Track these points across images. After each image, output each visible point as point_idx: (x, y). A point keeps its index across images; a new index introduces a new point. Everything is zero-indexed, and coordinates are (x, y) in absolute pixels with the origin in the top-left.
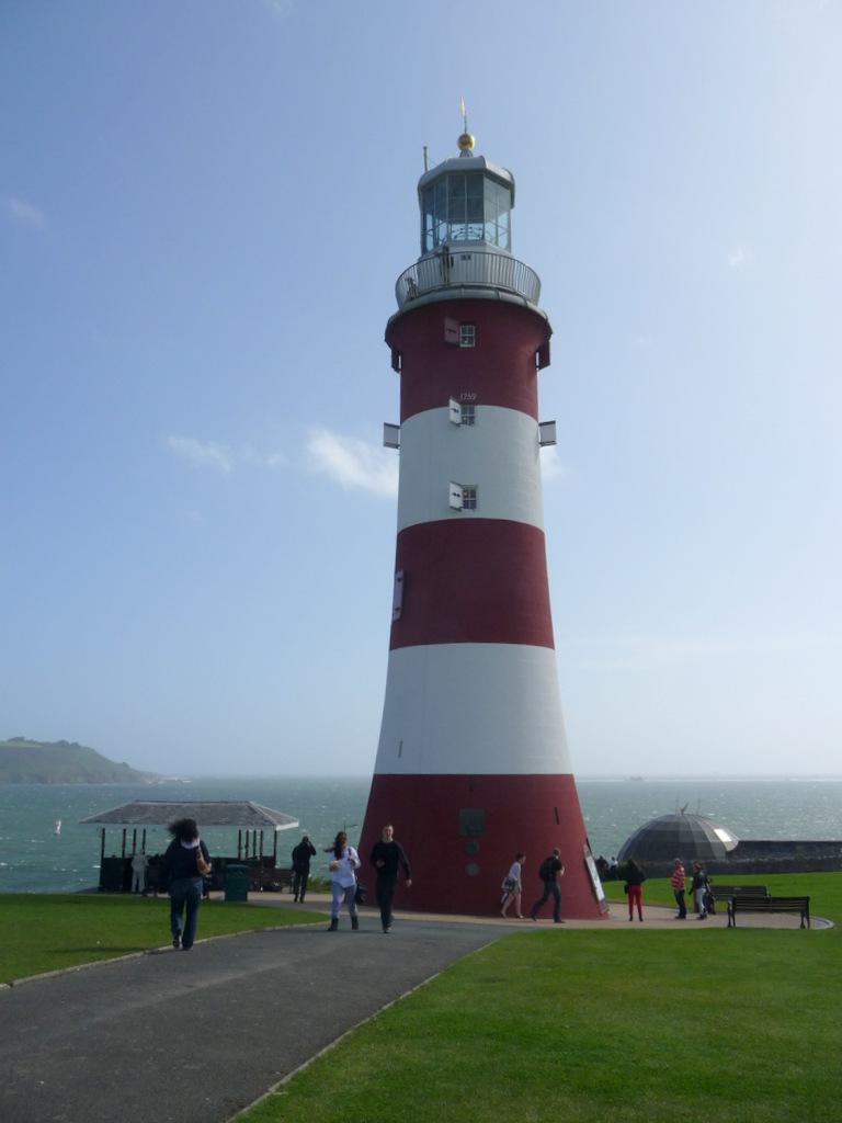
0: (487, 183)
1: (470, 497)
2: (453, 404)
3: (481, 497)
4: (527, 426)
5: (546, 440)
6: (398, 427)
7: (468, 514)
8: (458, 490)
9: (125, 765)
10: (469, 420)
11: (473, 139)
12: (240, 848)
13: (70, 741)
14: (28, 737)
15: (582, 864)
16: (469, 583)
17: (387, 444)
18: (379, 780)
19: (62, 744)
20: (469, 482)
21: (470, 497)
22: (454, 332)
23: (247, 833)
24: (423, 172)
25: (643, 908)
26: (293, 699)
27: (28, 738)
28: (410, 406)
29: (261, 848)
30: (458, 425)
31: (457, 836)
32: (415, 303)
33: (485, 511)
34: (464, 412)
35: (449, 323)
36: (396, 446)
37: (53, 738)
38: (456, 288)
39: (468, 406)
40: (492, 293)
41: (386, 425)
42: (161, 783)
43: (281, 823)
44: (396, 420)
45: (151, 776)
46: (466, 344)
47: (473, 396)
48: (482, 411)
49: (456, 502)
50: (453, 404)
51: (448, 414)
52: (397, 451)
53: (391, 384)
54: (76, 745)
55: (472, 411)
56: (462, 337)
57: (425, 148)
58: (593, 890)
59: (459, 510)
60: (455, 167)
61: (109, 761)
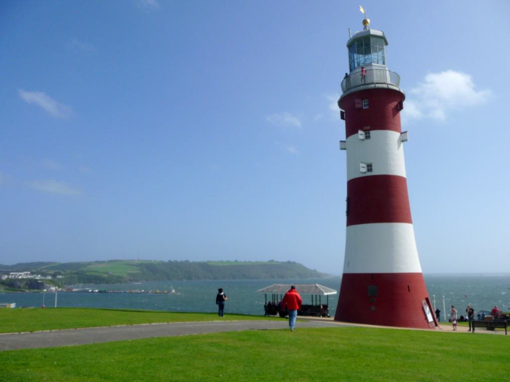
0: (372, 40)
1: (370, 167)
2: (360, 132)
3: (374, 168)
4: (394, 136)
5: (404, 139)
6: (345, 142)
7: (369, 174)
8: (365, 165)
9: (315, 270)
10: (368, 137)
11: (368, 20)
12: (312, 301)
13: (292, 261)
14: (276, 260)
15: (421, 308)
16: (374, 200)
17: (342, 149)
18: (345, 276)
19: (289, 262)
20: (369, 162)
21: (370, 167)
22: (360, 103)
23: (316, 296)
24: (349, 38)
25: (507, 332)
26: (321, 246)
27: (275, 260)
28: (351, 130)
29: (320, 300)
30: (363, 140)
31: (375, 297)
32: (348, 92)
33: (376, 172)
34: (366, 134)
35: (357, 101)
36: (345, 149)
37: (285, 260)
38: (354, 87)
39: (367, 132)
40: (373, 85)
41: (341, 141)
42: (325, 278)
43: (327, 292)
44: (344, 138)
45: (326, 275)
46: (370, 108)
47: (368, 128)
48: (373, 133)
49: (364, 170)
50: (360, 132)
51: (358, 137)
52: (345, 151)
53: (341, 126)
54: (294, 263)
55: (369, 133)
56: (365, 105)
57: (349, 29)
58: (426, 318)
59: (365, 173)
60: (360, 36)
61: (307, 269)
